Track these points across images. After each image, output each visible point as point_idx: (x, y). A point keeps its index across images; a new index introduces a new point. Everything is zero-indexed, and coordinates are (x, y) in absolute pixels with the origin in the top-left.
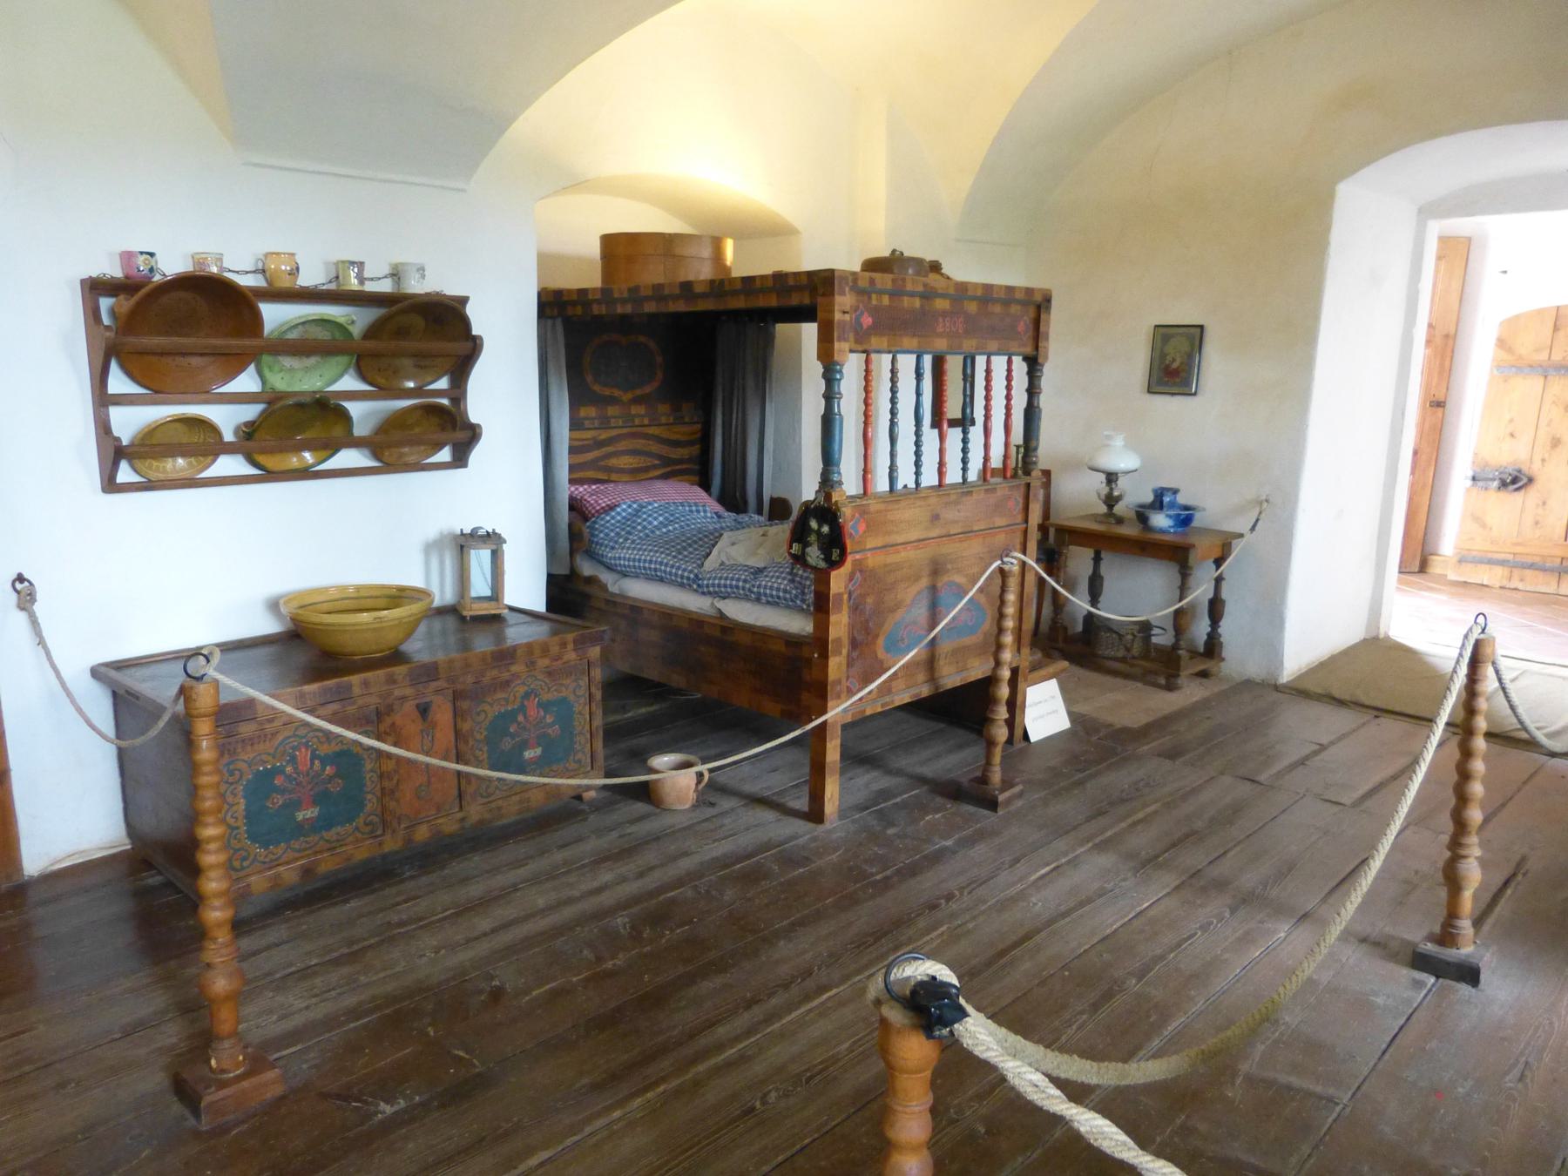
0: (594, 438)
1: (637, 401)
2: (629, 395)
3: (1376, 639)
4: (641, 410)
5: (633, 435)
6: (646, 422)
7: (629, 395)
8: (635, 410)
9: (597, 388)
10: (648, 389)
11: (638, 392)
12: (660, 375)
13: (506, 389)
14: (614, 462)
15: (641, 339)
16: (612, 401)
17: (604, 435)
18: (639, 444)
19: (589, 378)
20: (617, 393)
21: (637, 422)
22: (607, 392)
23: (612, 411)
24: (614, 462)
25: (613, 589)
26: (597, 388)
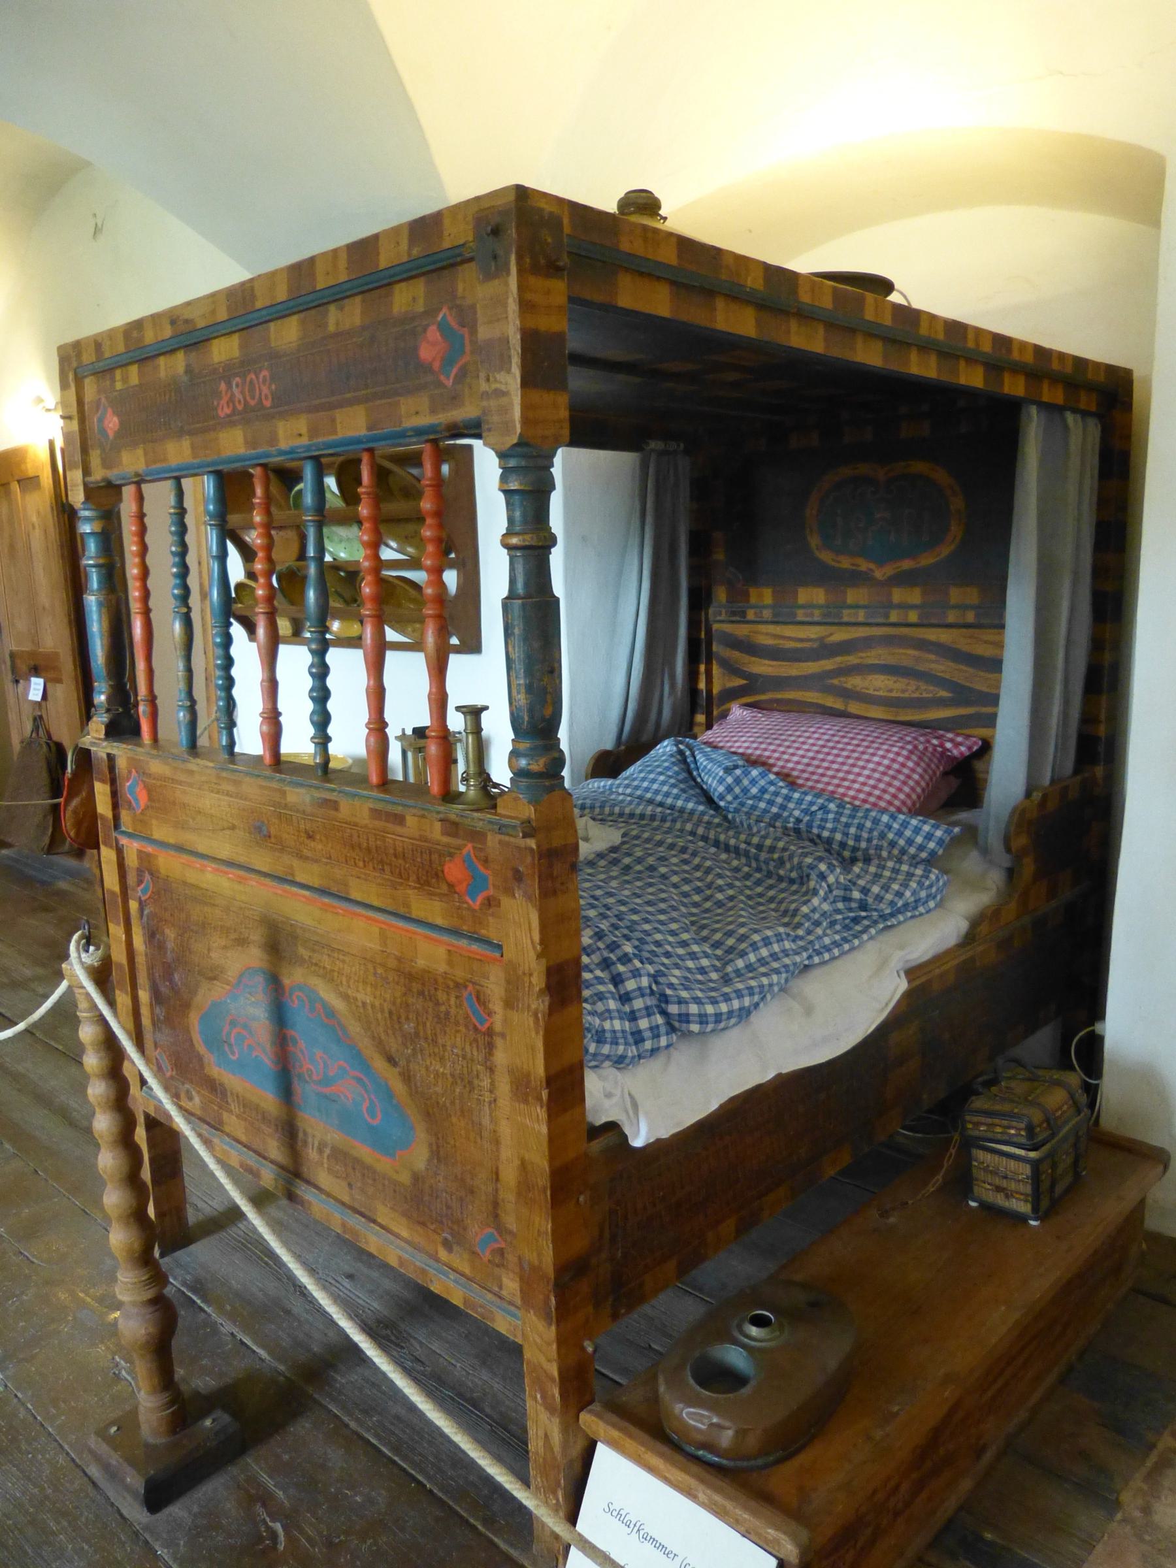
0: (821, 639)
1: (905, 579)
2: (888, 571)
3: (80, 1022)
4: (915, 596)
5: (888, 641)
6: (913, 617)
7: (888, 571)
8: (897, 595)
9: (826, 557)
10: (927, 560)
11: (907, 565)
12: (957, 503)
13: (733, 975)
14: (855, 682)
15: (919, 467)
16: (856, 578)
17: (839, 635)
18: (906, 656)
19: (814, 541)
20: (864, 565)
21: (894, 617)
22: (845, 563)
23: (853, 595)
24: (855, 682)
25: (529, 1404)
26: (826, 557)
